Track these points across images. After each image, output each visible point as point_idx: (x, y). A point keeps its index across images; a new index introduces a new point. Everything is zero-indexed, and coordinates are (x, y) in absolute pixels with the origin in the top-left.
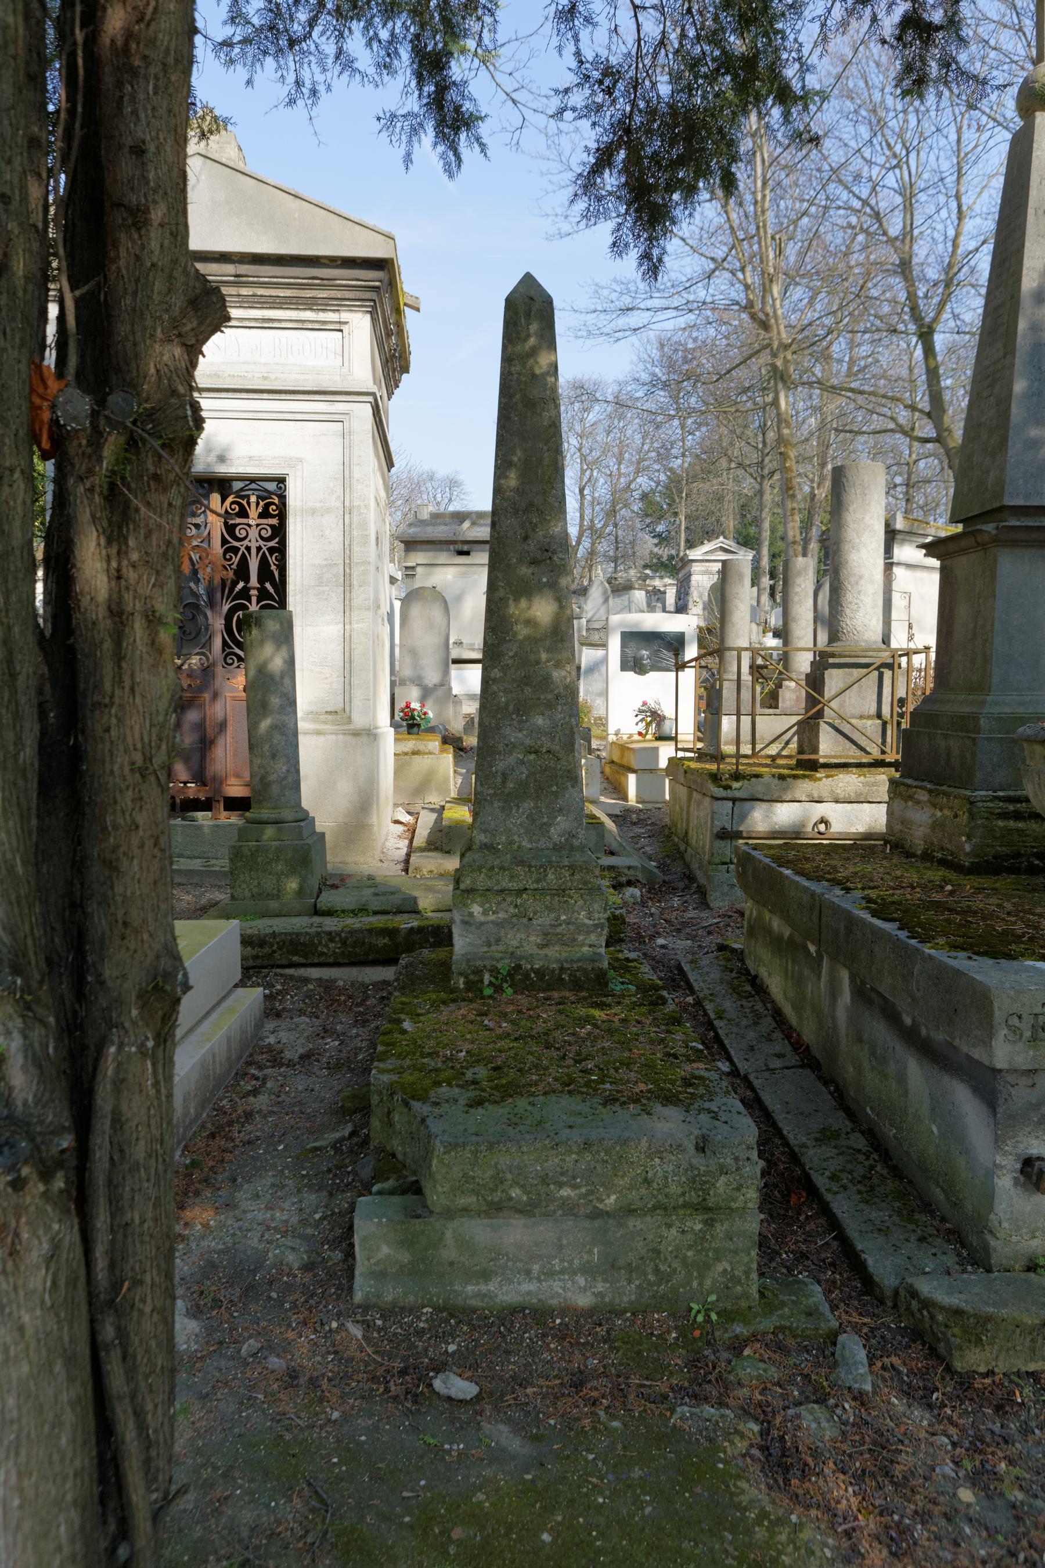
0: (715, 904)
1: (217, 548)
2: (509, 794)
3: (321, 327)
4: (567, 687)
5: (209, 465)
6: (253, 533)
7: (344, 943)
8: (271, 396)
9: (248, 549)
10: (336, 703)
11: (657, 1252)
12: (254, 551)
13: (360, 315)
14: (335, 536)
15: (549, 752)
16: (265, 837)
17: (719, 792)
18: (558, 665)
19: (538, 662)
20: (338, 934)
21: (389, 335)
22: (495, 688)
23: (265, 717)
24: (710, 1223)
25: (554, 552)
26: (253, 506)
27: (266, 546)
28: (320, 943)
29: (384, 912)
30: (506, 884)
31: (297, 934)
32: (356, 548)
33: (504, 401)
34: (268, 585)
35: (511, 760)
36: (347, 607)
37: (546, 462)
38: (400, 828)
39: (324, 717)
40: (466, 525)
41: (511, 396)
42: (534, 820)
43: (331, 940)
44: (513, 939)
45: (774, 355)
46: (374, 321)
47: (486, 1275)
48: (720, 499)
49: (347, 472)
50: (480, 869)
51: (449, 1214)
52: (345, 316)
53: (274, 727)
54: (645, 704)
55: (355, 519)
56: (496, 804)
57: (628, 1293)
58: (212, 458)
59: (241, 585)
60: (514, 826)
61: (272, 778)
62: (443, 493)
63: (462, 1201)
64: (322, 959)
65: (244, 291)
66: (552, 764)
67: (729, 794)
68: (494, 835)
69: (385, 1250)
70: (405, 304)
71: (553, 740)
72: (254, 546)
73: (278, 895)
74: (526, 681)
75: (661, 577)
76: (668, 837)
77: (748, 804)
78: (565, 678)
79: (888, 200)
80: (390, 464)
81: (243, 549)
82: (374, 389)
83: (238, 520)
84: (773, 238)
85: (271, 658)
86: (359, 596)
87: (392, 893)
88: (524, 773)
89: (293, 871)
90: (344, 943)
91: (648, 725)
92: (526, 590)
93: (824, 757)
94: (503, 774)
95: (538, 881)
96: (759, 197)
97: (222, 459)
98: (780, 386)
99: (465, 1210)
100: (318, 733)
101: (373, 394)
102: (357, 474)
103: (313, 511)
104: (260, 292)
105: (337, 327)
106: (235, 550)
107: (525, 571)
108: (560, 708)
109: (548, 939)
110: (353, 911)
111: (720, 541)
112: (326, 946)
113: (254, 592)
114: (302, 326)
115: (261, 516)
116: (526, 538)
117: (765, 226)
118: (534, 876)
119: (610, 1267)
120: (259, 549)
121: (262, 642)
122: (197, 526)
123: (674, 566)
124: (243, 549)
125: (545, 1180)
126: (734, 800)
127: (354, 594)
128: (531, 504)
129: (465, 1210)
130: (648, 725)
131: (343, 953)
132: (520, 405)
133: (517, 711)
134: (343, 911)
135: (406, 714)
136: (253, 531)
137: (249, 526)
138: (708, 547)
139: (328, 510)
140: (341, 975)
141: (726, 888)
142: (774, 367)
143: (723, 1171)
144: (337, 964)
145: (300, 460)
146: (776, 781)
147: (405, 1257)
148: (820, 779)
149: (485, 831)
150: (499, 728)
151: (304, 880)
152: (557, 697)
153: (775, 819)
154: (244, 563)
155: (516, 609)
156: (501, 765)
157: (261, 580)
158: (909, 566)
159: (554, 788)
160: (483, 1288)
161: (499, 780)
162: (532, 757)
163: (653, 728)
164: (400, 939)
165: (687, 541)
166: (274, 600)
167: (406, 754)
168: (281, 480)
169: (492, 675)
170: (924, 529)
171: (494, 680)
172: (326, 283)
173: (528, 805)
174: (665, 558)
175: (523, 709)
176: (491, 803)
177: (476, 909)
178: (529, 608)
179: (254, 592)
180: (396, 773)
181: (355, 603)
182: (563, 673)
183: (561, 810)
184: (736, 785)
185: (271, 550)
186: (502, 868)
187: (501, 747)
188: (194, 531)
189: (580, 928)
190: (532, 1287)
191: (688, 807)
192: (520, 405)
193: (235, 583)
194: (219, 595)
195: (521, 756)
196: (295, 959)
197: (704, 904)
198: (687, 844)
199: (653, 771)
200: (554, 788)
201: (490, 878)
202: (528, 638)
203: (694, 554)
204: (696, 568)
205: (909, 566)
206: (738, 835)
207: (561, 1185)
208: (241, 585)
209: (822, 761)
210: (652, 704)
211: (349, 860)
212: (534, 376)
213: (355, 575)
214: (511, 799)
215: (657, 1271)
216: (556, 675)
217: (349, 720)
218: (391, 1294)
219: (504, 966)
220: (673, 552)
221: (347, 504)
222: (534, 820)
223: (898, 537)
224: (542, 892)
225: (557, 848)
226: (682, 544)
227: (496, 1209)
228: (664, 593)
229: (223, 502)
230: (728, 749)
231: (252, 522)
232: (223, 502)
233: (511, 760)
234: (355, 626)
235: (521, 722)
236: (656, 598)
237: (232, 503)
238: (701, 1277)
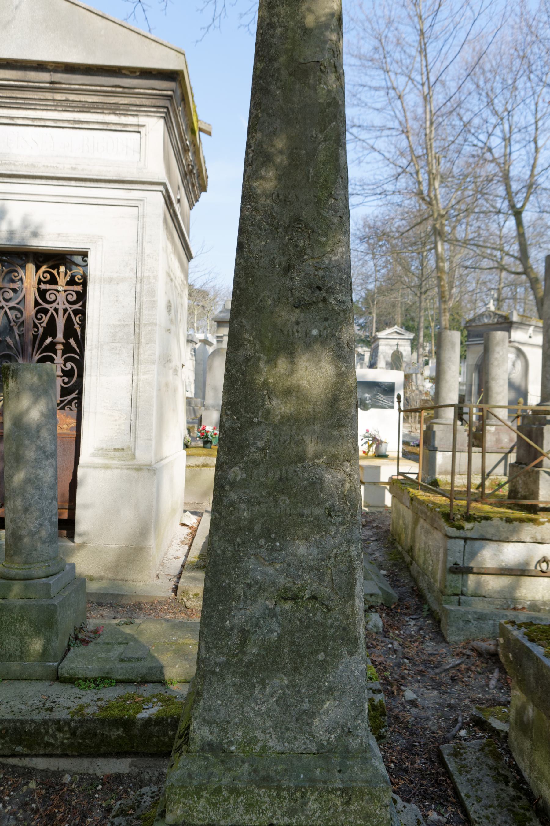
0: (451, 638)
1: (30, 310)
2: (250, 663)
3: (123, 129)
4: (345, 497)
5: (23, 239)
6: (61, 297)
7: (74, 734)
8: (78, 184)
9: (56, 310)
10: (123, 441)
12: (61, 312)
13: (155, 120)
14: (128, 301)
15: (314, 598)
16: (13, 594)
17: (452, 532)
18: (333, 463)
19: (301, 458)
20: (67, 723)
21: (186, 150)
22: (233, 496)
23: (17, 469)
25: (331, 291)
26: (62, 275)
27: (71, 308)
28: (47, 732)
29: (128, 682)
31: (22, 722)
32: (145, 312)
33: (261, 66)
34: (72, 341)
35: (255, 609)
36: (135, 360)
37: (321, 157)
38: (186, 531)
39: (112, 453)
41: (272, 60)
42: (287, 707)
43: (60, 730)
45: (436, 220)
46: (169, 127)
48: (394, 306)
49: (140, 248)
50: (198, 791)
52: (142, 120)
53: (28, 481)
54: (368, 431)
55: (145, 287)
56: (230, 680)
58: (27, 233)
59: (49, 340)
61: (23, 532)
64: (49, 750)
65: (58, 97)
66: (319, 617)
67: (461, 533)
68: (225, 730)
70: (200, 130)
71: (321, 579)
72: (61, 308)
73: (22, 655)
74: (282, 486)
75: (362, 347)
76: (393, 543)
77: (478, 543)
78: (343, 482)
79: (496, 142)
80: (190, 257)
81: (52, 310)
82: (163, 178)
83: (48, 287)
84: (435, 157)
85: (28, 410)
86: (146, 352)
87: (139, 660)
88: (274, 631)
89: (38, 632)
91: (370, 446)
92: (286, 346)
93: (542, 502)
94: (243, 631)
95: (291, 813)
96: (428, 131)
97: (35, 234)
98: (438, 238)
100: (106, 467)
101: (164, 184)
102: (148, 249)
103: (111, 280)
104: (72, 97)
105: (136, 129)
107: (287, 316)
108: (333, 529)
110: (95, 680)
111: (396, 328)
112: (54, 736)
113: (60, 347)
114: (106, 127)
115: (68, 283)
116: (288, 269)
117: (431, 148)
118: (286, 804)
120: (65, 310)
121: (18, 395)
122: (15, 291)
123: (369, 342)
124: (52, 310)
126: (466, 539)
127: (141, 350)
128: (298, 219)
130: (370, 446)
131: (72, 744)
132: (284, 72)
133: (267, 533)
134: (85, 679)
135: (202, 434)
136: (61, 295)
137: (58, 291)
138: (388, 331)
140: (70, 767)
141: (461, 624)
144: (64, 755)
145: (101, 238)
146: (504, 523)
148: (543, 523)
149: (210, 723)
150: (237, 559)
151: (48, 642)
152: (330, 512)
153: (502, 557)
154: (52, 322)
155: (275, 372)
156: (238, 617)
159: (321, 656)
161: (235, 640)
162: (288, 606)
163: (374, 448)
164: (136, 731)
165: (376, 328)
166: (76, 353)
167: (198, 466)
168: (84, 254)
169: (231, 476)
170: (529, 321)
171: (233, 484)
172: (127, 91)
173: (279, 681)
174: (363, 337)
175: (276, 531)
176: (222, 677)
178: (292, 372)
179: (60, 347)
180: (187, 481)
181: (142, 357)
182: (340, 476)
183: (331, 690)
184: (467, 526)
185: (76, 312)
186: (234, 791)
187: (240, 589)
188: (12, 294)
191: (413, 531)
192: (284, 72)
193: (44, 338)
194: (30, 349)
195: (270, 604)
196: (19, 749)
197: (440, 636)
198: (413, 558)
199: (376, 483)
200: (321, 656)
201: (214, 806)
202: (287, 420)
203: (380, 335)
204: (381, 342)
206: (469, 570)
208: (49, 340)
209: (541, 505)
210: (373, 433)
211: (129, 577)
212: (306, 31)
213: (143, 334)
214: (252, 673)
216: (330, 478)
217: (134, 457)
220: (368, 334)
221: (139, 275)
222: (287, 707)
223: (515, 325)
225: (323, 753)
226: (374, 329)
228: (364, 355)
229: (37, 271)
230: (443, 478)
231: (59, 288)
232: (37, 271)
233: (255, 609)
234: (142, 377)
235: (273, 549)
237: (45, 272)
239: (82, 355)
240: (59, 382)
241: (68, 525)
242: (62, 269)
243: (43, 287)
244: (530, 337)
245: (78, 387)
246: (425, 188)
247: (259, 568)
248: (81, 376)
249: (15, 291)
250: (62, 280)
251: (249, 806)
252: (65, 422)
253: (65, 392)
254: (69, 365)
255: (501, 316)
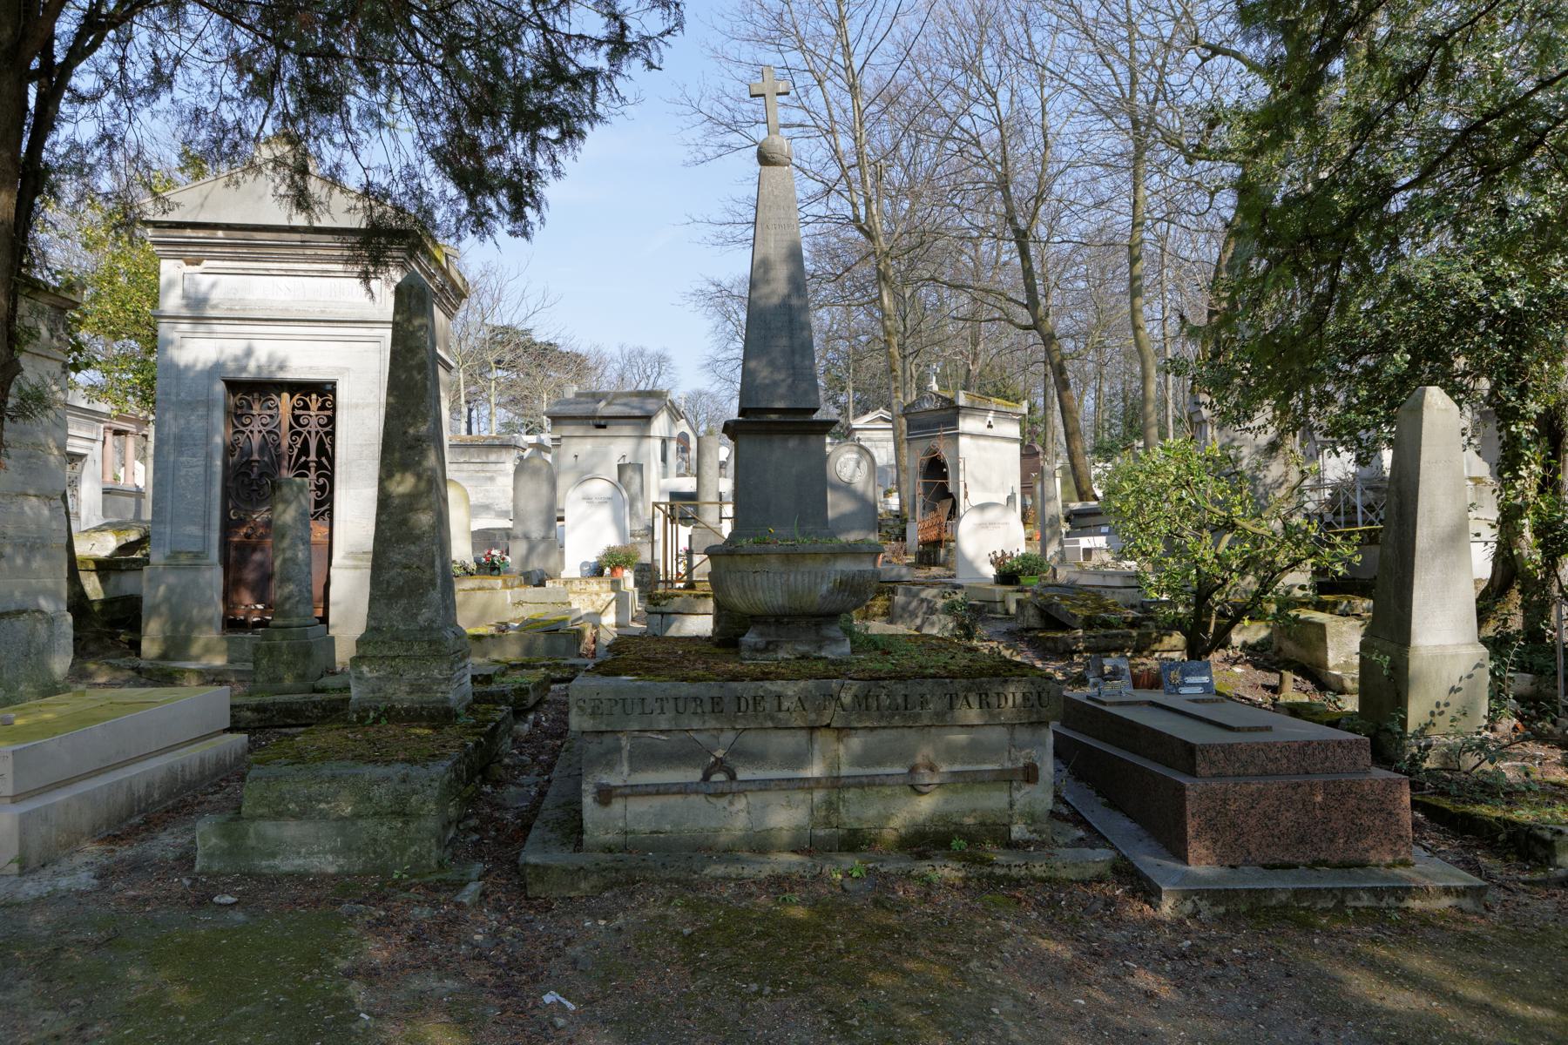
6: (314, 421)
11: (375, 840)
24: (406, 823)
30: (385, 652)
40: (603, 404)
44: (390, 689)
47: (273, 855)
51: (253, 818)
57: (358, 864)
60: (395, 616)
62: (652, 367)
63: (260, 811)
65: (308, 252)
67: (658, 609)
69: (214, 840)
90: (324, 709)
97: (281, 368)
99: (262, 816)
100: (356, 567)
103: (357, 406)
106: (299, 434)
109: (416, 688)
115: (320, 409)
119: (346, 850)
125: (309, 798)
126: (662, 614)
129: (262, 816)
138: (871, 416)
139: (368, 405)
142: (879, 270)
143: (415, 792)
147: (225, 844)
154: (306, 443)
157: (318, 455)
158: (972, 435)
160: (272, 862)
168: (334, 384)
177: (365, 669)
185: (327, 434)
189: (435, 681)
190: (301, 862)
205: (972, 435)
207: (320, 802)
215: (375, 852)
218: (216, 867)
219: (382, 706)
224: (409, 657)
225: (422, 629)
227: (278, 815)
233: (393, 573)
236: (679, 467)
238: (402, 855)
239: (333, 471)
240: (313, 496)
241: (324, 619)
242: (314, 396)
243: (297, 412)
244: (990, 426)
245: (330, 500)
246: (862, 211)
247: (396, 556)
248: (332, 491)
249: (271, 416)
250: (314, 406)
251: (390, 648)
252: (318, 531)
253: (318, 504)
254: (321, 481)
255: (945, 399)
